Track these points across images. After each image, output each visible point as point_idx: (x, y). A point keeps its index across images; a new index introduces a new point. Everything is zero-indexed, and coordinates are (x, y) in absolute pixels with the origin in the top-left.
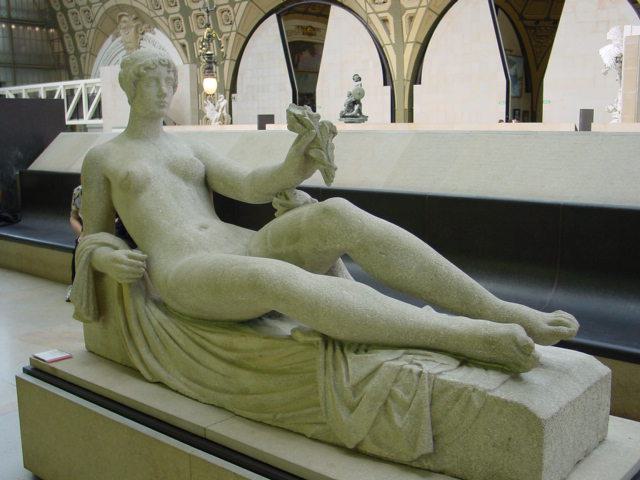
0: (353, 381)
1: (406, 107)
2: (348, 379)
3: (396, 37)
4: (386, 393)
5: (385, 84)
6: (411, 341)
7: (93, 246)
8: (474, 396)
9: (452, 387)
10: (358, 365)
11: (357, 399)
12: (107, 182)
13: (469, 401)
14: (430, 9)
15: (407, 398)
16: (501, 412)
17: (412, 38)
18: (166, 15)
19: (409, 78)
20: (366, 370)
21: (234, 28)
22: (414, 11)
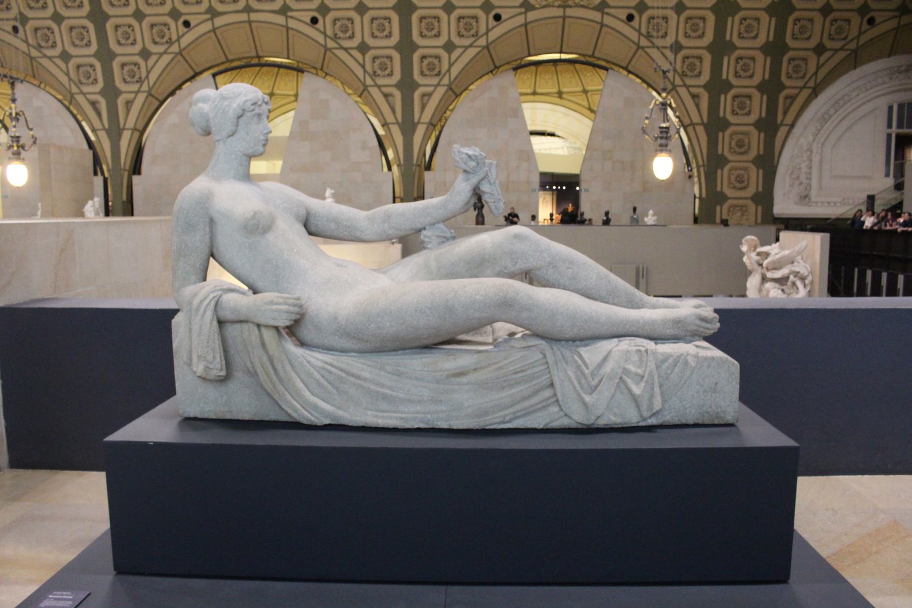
0: (591, 368)
1: (124, 198)
2: (588, 368)
3: (403, 116)
4: (620, 371)
5: (96, 174)
6: (621, 331)
7: (220, 293)
8: (689, 358)
9: (671, 356)
10: (591, 354)
11: (596, 381)
12: (212, 222)
13: (686, 363)
14: (451, 89)
15: (640, 371)
16: (709, 366)
17: (130, 124)
18: (66, 56)
19: (127, 167)
20: (600, 357)
21: (145, 87)
22: (132, 96)
